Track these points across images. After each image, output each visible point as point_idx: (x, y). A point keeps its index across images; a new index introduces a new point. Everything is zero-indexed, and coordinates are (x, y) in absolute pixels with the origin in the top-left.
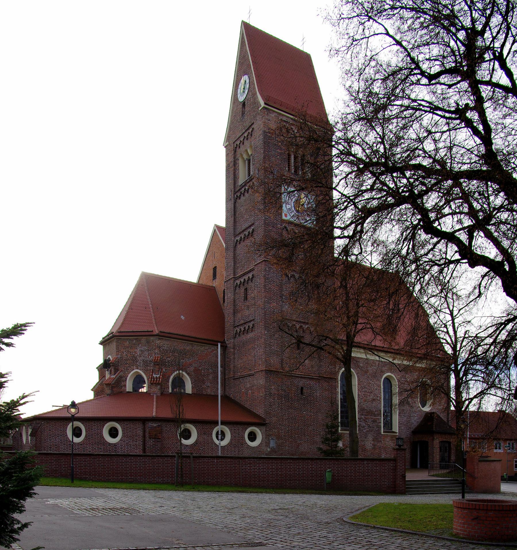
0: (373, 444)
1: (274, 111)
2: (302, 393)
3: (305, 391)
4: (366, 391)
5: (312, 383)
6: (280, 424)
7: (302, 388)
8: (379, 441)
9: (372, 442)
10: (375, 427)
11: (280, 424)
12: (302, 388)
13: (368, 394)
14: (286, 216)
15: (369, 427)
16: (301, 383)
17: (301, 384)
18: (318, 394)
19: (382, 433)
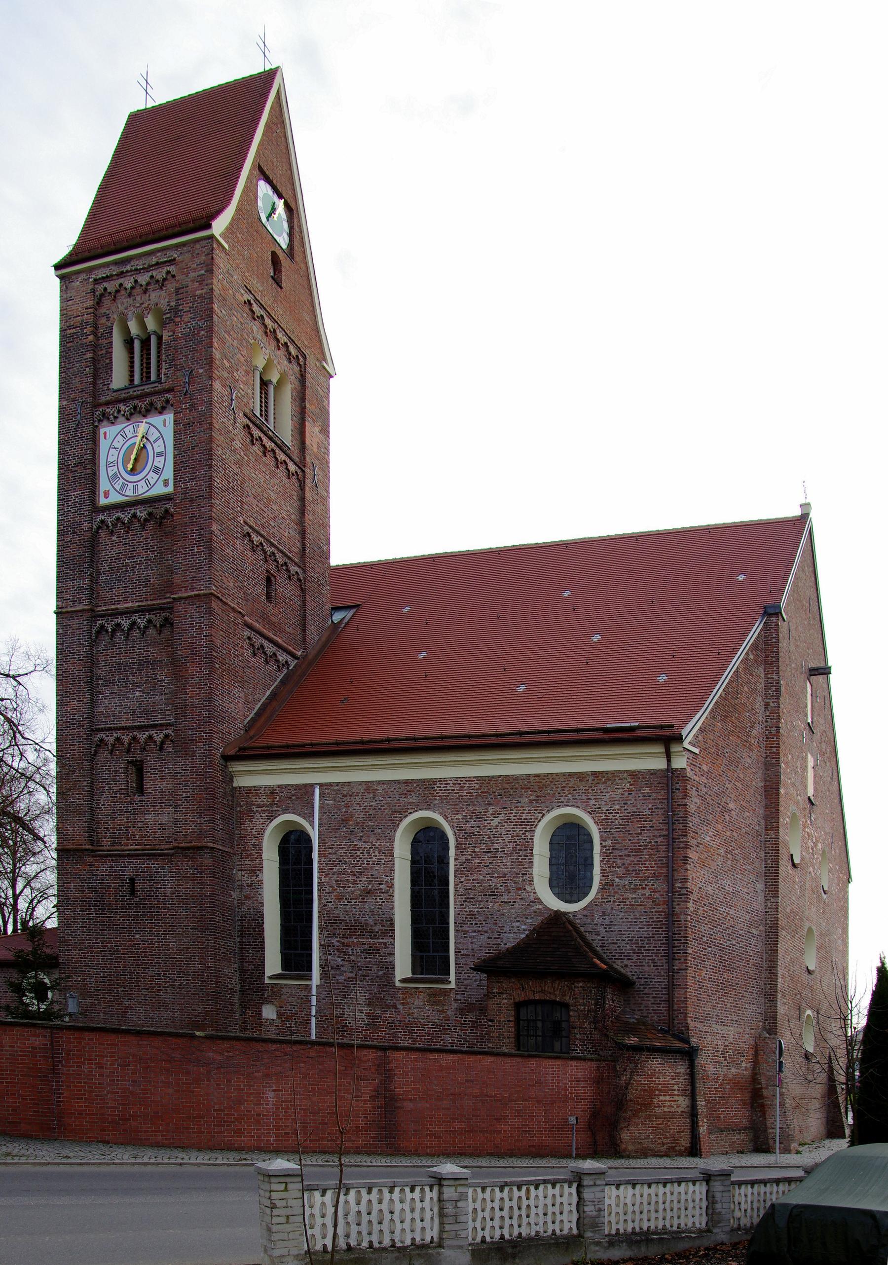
0: (368, 1015)
1: (78, 272)
2: (133, 892)
3: (138, 886)
4: (344, 872)
5: (154, 865)
6: (87, 965)
7: (132, 881)
8: (388, 1007)
9: (366, 1009)
10: (375, 968)
11: (87, 965)
12: (132, 881)
13: (351, 878)
14: (107, 495)
15: (354, 965)
16: (130, 868)
17: (129, 872)
18: (169, 891)
19: (398, 984)
